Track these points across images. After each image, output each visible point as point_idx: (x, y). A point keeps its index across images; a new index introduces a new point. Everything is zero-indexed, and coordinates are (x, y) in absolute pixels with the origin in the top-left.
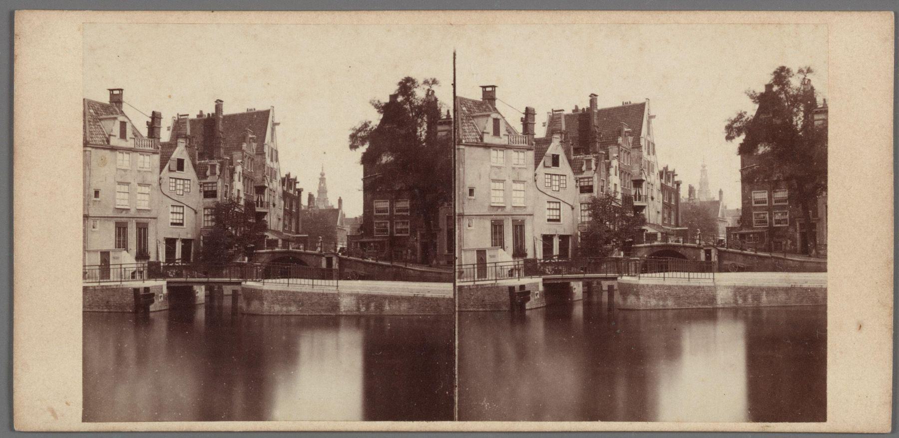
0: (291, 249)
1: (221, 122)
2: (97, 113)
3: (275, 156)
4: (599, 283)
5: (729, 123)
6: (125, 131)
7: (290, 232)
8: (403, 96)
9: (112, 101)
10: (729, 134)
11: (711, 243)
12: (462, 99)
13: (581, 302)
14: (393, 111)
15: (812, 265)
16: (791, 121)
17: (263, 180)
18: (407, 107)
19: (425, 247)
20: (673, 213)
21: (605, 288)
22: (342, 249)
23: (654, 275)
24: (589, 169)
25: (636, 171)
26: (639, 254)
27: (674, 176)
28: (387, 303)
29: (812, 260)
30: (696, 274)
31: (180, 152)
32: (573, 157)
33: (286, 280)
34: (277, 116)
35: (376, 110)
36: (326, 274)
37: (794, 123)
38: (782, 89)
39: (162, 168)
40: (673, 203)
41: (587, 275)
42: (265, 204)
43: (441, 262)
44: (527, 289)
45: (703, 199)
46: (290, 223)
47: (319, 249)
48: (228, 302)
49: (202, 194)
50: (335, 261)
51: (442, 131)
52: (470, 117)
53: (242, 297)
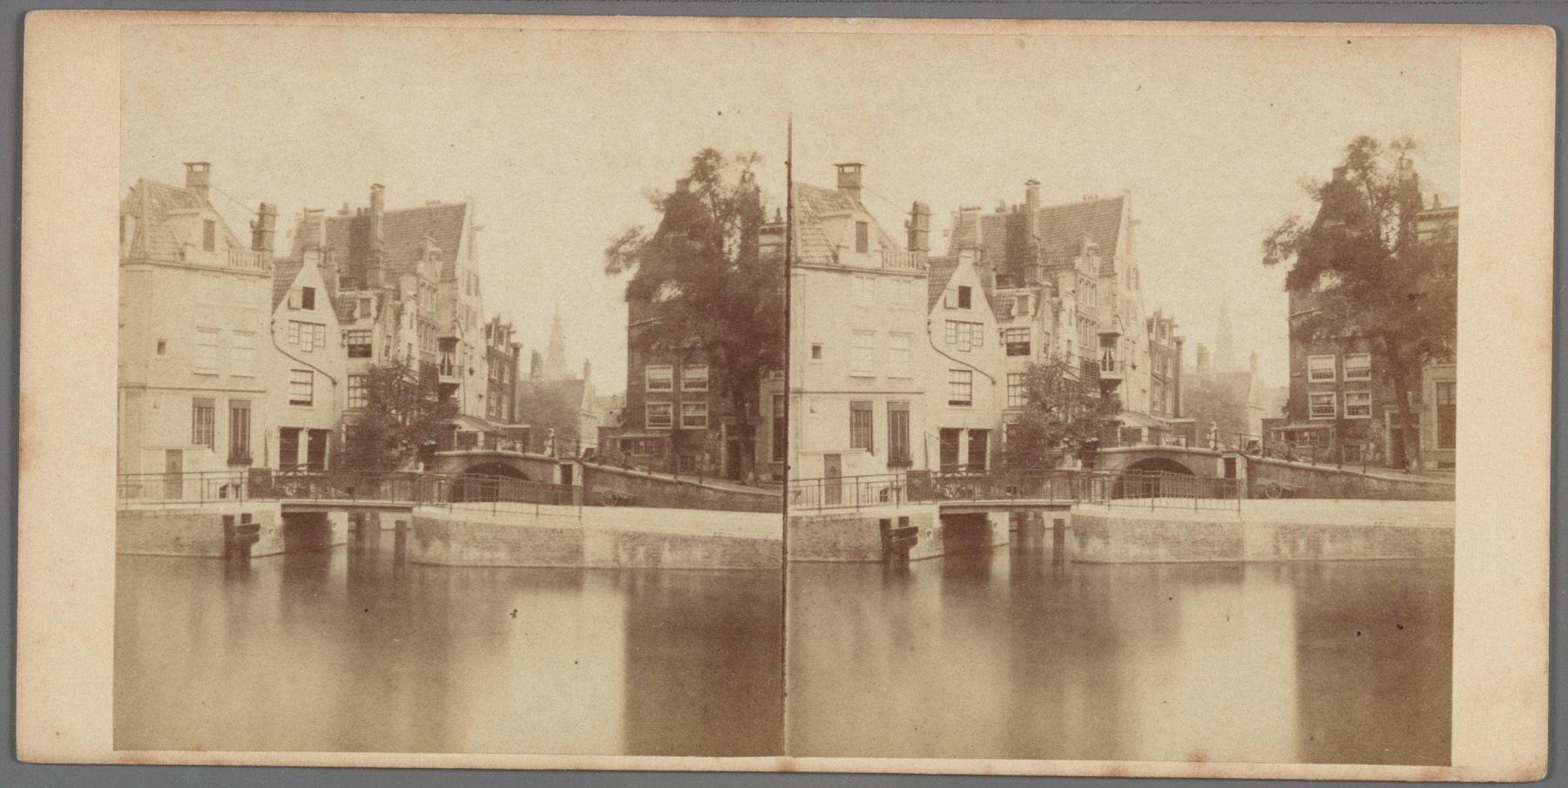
0: (499, 450)
1: (1036, 221)
3: (475, 289)
4: (1037, 516)
6: (865, 241)
7: (498, 418)
8: (700, 180)
9: (190, 183)
10: (1270, 254)
11: (1236, 448)
16: (1378, 234)
18: (707, 201)
19: (734, 448)
21: (1049, 523)
22: (589, 451)
23: (1134, 501)
25: (444, 322)
27: (1171, 327)
28: (667, 544)
29: (1412, 478)
32: (995, 292)
33: (489, 505)
34: (476, 216)
36: (561, 496)
37: (1383, 237)
39: (932, 303)
40: (506, 381)
41: (1020, 501)
42: (455, 370)
43: (763, 477)
46: (499, 400)
47: (548, 451)
48: (387, 543)
49: (346, 350)
50: (577, 472)
51: (767, 246)
52: (815, 218)
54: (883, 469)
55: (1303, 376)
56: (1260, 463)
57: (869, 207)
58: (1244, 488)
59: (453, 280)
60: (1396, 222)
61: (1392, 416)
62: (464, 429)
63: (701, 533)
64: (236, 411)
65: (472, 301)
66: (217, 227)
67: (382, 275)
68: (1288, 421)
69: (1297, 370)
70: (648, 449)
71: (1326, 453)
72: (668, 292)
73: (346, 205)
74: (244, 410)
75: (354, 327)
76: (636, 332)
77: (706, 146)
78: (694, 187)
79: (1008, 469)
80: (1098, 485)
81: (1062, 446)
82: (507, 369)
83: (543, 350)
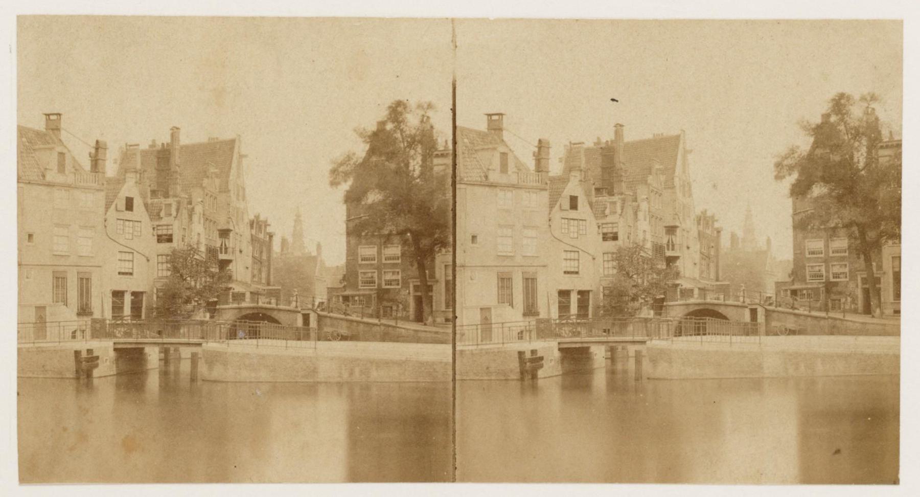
1: (177, 153)
2: (30, 142)
3: (242, 194)
5: (335, 166)
7: (260, 282)
8: (393, 122)
11: (757, 301)
12: (463, 129)
13: (604, 370)
14: (381, 142)
15: (429, 335)
16: (852, 157)
17: (228, 223)
19: (419, 301)
20: (712, 265)
22: (321, 303)
23: (689, 338)
29: (875, 321)
30: (739, 337)
32: (594, 199)
33: (254, 341)
35: (360, 140)
36: (303, 334)
37: (856, 160)
38: (842, 120)
39: (551, 207)
42: (230, 250)
44: (95, 354)
45: (298, 253)
46: (260, 271)
47: (294, 304)
48: (185, 367)
49: (601, 236)
53: (203, 360)
54: (519, 317)
55: (803, 253)
56: (774, 311)
57: (509, 143)
58: (763, 329)
59: (673, 187)
60: (864, 150)
61: (414, 286)
62: (236, 290)
63: (403, 357)
65: (241, 205)
66: (68, 156)
67: (179, 188)
68: (793, 282)
69: (798, 249)
71: (818, 305)
72: (373, 197)
73: (154, 141)
74: (87, 279)
75: (161, 223)
76: (351, 225)
77: (841, 91)
78: (389, 126)
79: (604, 316)
80: (665, 326)
81: (641, 301)
82: (264, 249)
83: (740, 234)
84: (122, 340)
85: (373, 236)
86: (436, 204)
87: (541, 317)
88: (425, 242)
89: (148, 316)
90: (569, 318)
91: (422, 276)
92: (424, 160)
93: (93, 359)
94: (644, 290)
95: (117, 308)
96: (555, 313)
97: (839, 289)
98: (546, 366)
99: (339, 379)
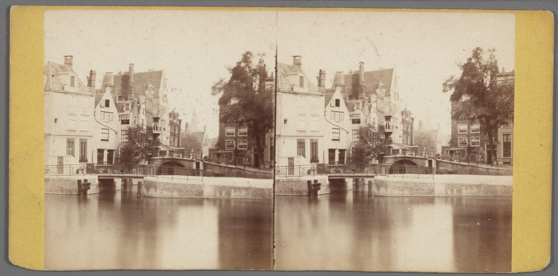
1: (363, 76)
2: (285, 71)
4: (363, 180)
7: (174, 146)
8: (245, 62)
10: (445, 88)
11: (432, 156)
13: (352, 191)
14: (238, 73)
15: (262, 174)
16: (483, 81)
19: (256, 157)
21: (367, 182)
22: (206, 157)
24: (358, 109)
25: (155, 112)
26: (156, 163)
27: (178, 116)
28: (464, 188)
29: (494, 167)
31: (108, 95)
32: (348, 101)
33: (401, 175)
35: (228, 71)
36: (195, 173)
37: (485, 82)
40: (177, 132)
41: (356, 174)
42: (159, 128)
44: (88, 182)
45: (194, 131)
46: (407, 139)
47: (191, 157)
48: (135, 189)
49: (120, 122)
50: (434, 162)
51: (268, 85)
52: (285, 75)
54: (309, 163)
55: (456, 131)
56: (441, 162)
59: (158, 97)
61: (487, 146)
63: (244, 186)
64: (82, 143)
65: (165, 105)
66: (305, 79)
68: (451, 146)
70: (226, 157)
71: (464, 159)
76: (222, 116)
81: (372, 155)
82: (177, 128)
84: (332, 175)
85: (233, 122)
86: (266, 105)
87: (88, 162)
88: (492, 122)
89: (116, 162)
90: (334, 163)
91: (258, 144)
92: (260, 82)
93: (87, 185)
94: (142, 151)
95: (100, 158)
96: (95, 161)
97: (475, 150)
98: (91, 188)
99: (446, 195)
